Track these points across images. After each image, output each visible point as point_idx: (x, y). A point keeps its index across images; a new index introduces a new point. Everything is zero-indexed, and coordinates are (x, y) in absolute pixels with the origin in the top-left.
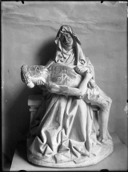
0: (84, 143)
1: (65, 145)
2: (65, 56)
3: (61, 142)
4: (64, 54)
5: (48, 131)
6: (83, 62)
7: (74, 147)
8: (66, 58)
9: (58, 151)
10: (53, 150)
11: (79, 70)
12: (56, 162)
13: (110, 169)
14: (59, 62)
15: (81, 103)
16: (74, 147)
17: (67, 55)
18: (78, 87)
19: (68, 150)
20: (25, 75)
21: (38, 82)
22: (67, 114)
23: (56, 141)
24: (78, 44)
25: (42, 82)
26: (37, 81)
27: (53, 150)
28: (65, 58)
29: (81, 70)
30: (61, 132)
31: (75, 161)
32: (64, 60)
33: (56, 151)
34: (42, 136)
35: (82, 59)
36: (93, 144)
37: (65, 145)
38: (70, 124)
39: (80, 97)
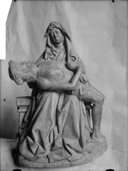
0: (78, 139)
1: (59, 144)
2: (54, 53)
3: (54, 141)
4: (53, 51)
5: (40, 159)
6: (73, 59)
7: (67, 145)
8: (55, 56)
9: (51, 150)
10: (45, 150)
11: (71, 66)
12: (49, 163)
13: (43, 3)
14: (49, 59)
15: (73, 98)
16: (67, 145)
17: (57, 52)
18: (70, 81)
19: (62, 148)
20: (13, 70)
21: (27, 78)
22: (59, 110)
23: (49, 142)
24: (67, 39)
25: (32, 78)
26: (26, 77)
27: (45, 150)
28: (55, 55)
29: (72, 66)
30: (53, 130)
31: (70, 159)
32: (54, 57)
33: (49, 149)
34: (33, 137)
35: (72, 55)
36: (87, 140)
37: (59, 144)
38: (62, 121)
39: (73, 93)
